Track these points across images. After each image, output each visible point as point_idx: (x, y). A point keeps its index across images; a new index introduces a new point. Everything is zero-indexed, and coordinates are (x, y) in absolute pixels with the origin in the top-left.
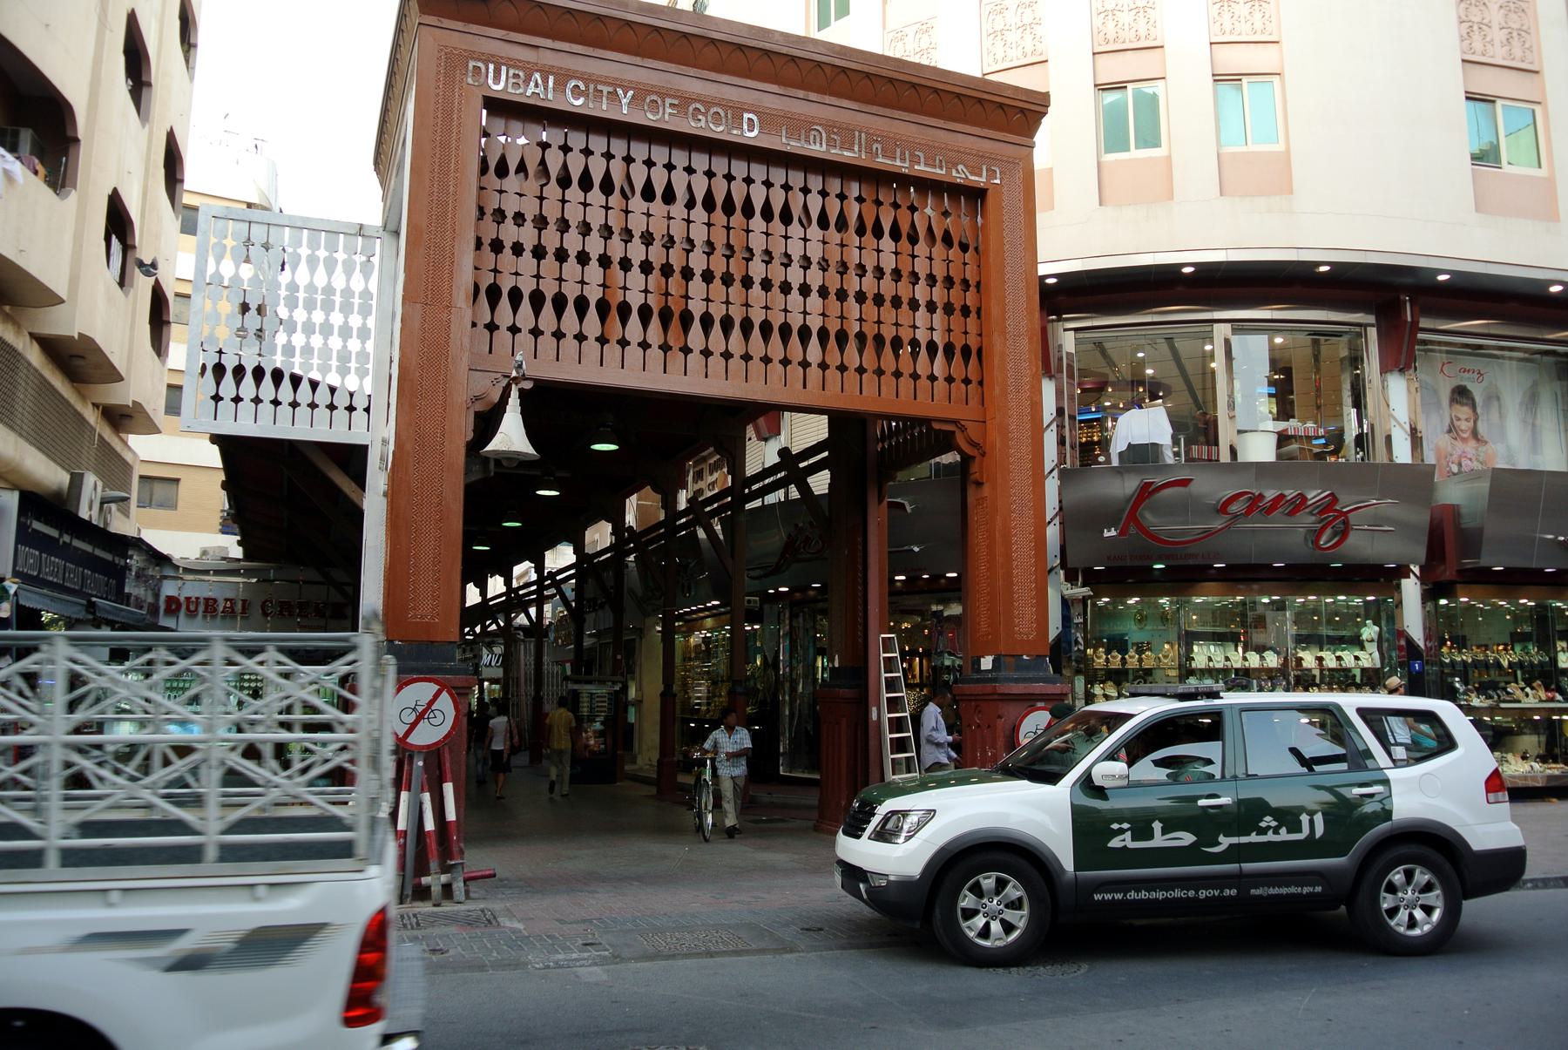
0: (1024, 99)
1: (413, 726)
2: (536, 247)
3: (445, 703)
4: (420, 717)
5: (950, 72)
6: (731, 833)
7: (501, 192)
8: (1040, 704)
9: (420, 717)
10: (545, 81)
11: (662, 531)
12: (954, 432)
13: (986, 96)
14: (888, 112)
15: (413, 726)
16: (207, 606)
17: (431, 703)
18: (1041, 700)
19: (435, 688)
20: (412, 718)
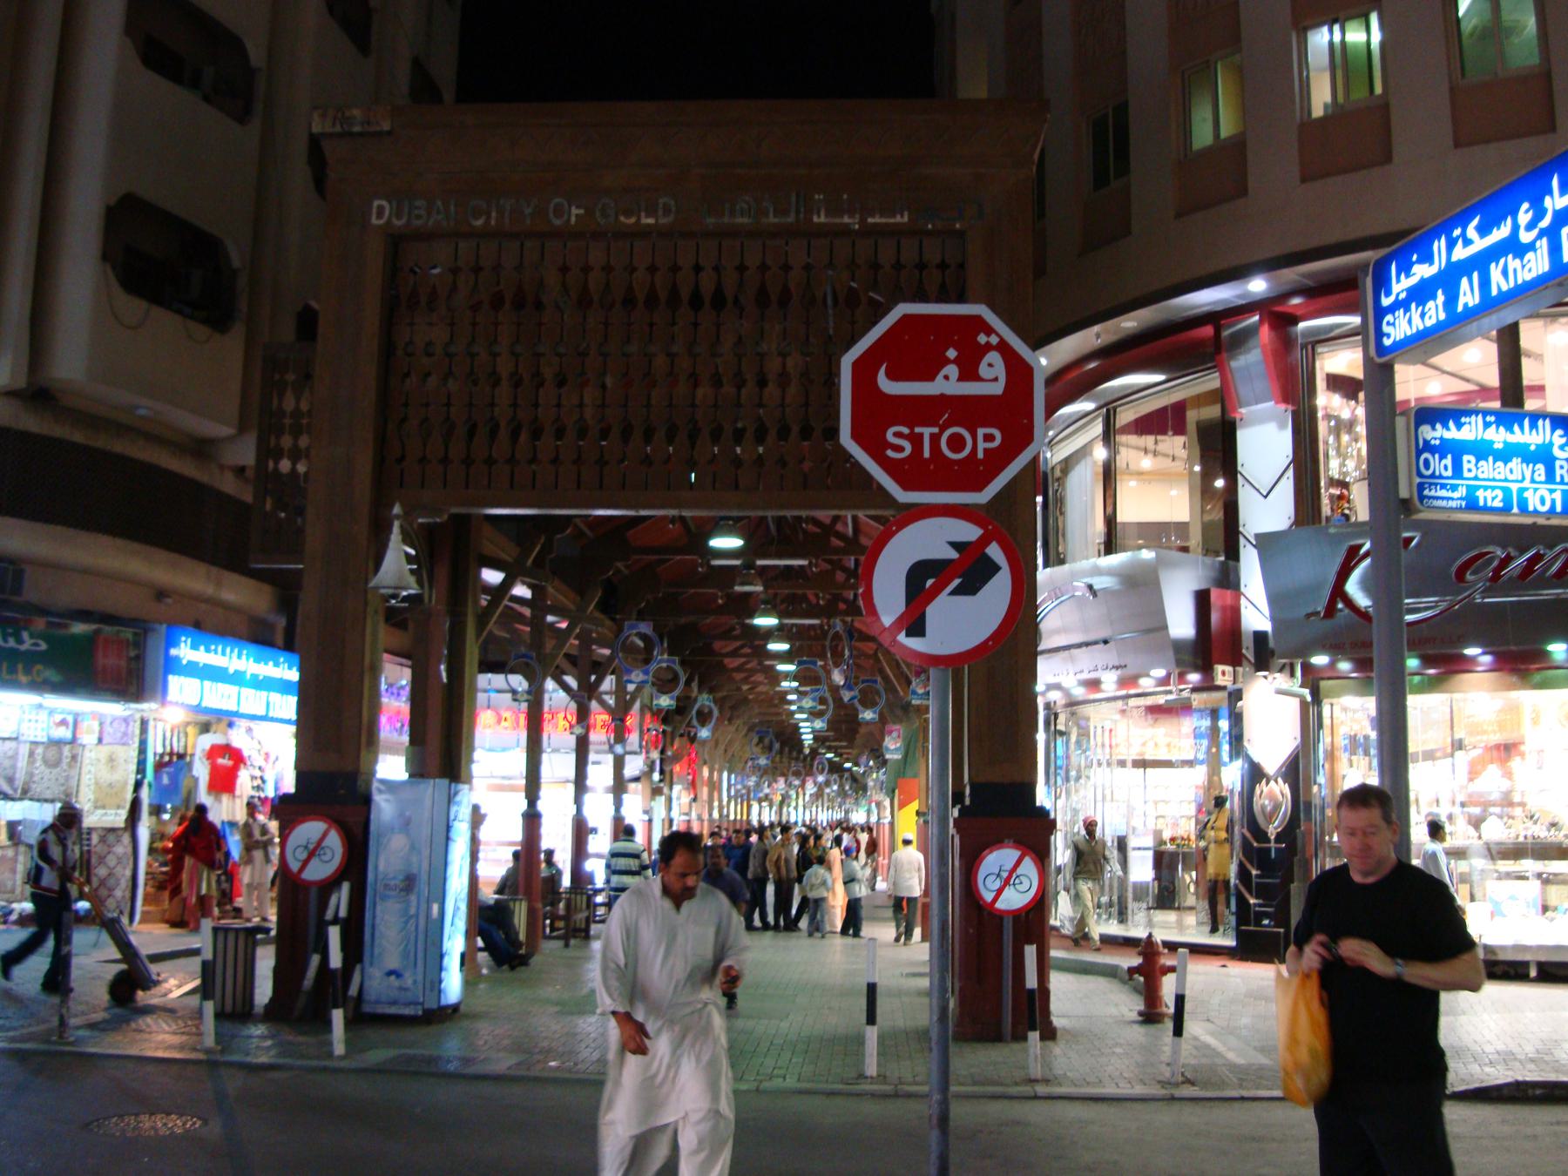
9: (1007, 882)
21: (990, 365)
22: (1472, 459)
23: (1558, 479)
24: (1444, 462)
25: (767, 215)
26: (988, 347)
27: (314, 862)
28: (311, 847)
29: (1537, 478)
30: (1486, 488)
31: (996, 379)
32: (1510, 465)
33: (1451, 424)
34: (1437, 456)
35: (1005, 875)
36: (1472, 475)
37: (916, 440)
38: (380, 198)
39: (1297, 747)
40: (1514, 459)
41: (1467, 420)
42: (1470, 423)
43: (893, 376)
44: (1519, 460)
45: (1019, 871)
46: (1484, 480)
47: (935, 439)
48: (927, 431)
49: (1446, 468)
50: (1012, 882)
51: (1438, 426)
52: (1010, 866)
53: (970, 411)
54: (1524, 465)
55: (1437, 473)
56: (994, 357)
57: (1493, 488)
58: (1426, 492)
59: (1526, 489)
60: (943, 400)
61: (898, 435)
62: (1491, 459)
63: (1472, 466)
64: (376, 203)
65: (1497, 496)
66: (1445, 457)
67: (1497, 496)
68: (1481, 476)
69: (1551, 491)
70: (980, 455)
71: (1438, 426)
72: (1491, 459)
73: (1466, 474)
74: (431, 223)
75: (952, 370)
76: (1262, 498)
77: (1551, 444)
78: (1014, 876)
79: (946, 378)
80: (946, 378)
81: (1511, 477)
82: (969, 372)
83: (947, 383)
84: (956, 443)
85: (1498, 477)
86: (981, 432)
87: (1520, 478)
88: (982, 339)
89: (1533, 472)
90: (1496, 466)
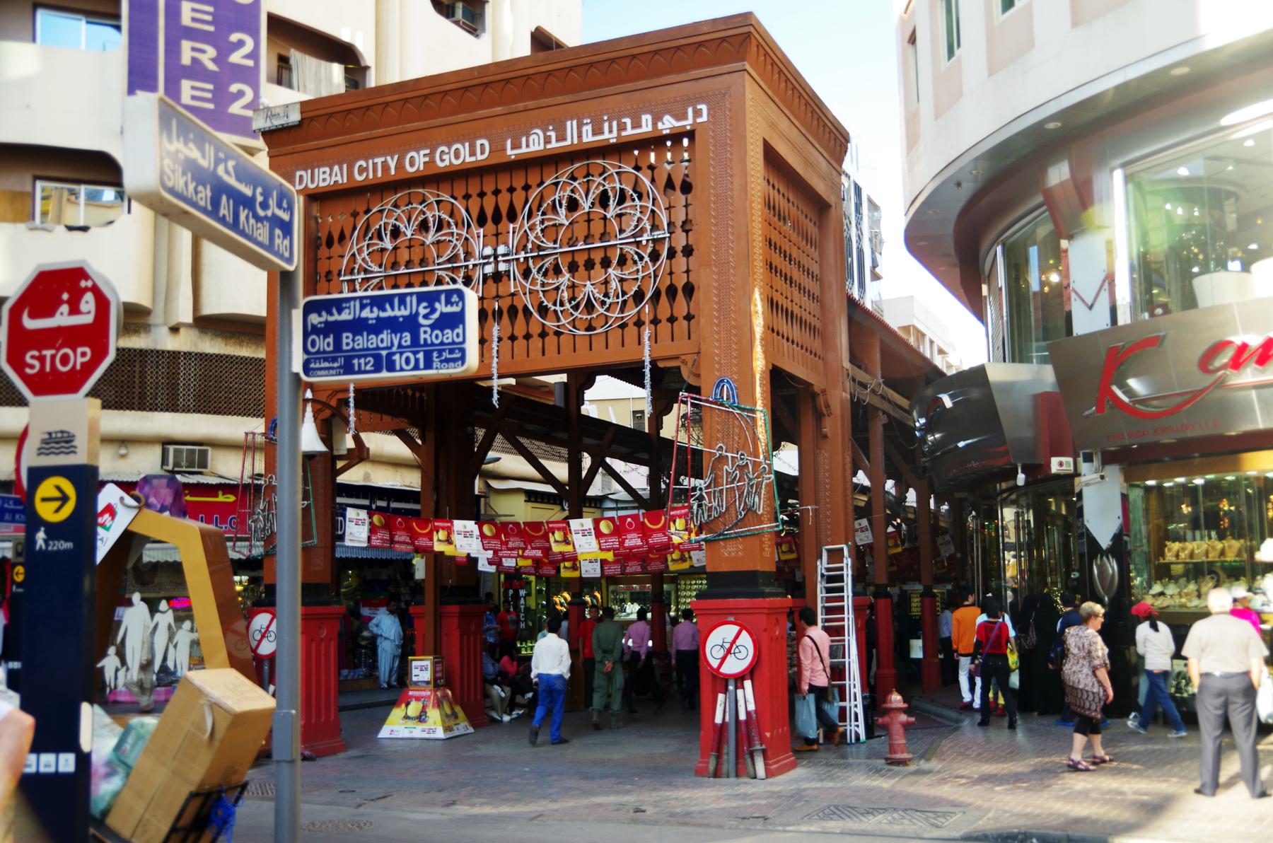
0: (724, 27)
1: (723, 659)
2: (684, 223)
3: (746, 640)
4: (729, 652)
5: (645, 34)
6: (1098, 762)
7: (329, 258)
8: (731, 619)
9: (729, 652)
10: (341, 169)
11: (961, 444)
12: (678, 368)
13: (682, 42)
14: (597, 92)
15: (723, 659)
16: (1242, 528)
17: (734, 642)
18: (731, 614)
19: (737, 628)
20: (721, 653)
21: (87, 302)
22: (350, 335)
23: (422, 342)
24: (327, 340)
25: (625, 129)
26: (86, 289)
27: (265, 641)
28: (263, 631)
29: (404, 343)
30: (359, 357)
31: (89, 312)
32: (381, 336)
33: (334, 311)
34: (322, 337)
35: (727, 646)
36: (349, 347)
37: (42, 359)
38: (300, 170)
39: (1121, 525)
40: (385, 332)
41: (348, 305)
42: (349, 308)
43: (33, 316)
44: (389, 331)
45: (738, 642)
46: (360, 350)
47: (53, 357)
48: (48, 353)
49: (328, 345)
50: (732, 652)
51: (324, 313)
52: (730, 639)
53: (72, 336)
54: (393, 335)
55: (322, 349)
56: (89, 297)
57: (365, 356)
58: (312, 366)
59: (394, 354)
60: (59, 330)
61: (33, 357)
62: (365, 334)
63: (350, 341)
64: (298, 174)
65: (369, 361)
66: (328, 337)
67: (369, 361)
68: (357, 347)
69: (415, 353)
70: (78, 367)
71: (324, 313)
72: (365, 334)
73: (345, 348)
74: (332, 183)
75: (65, 308)
76: (1086, 309)
77: (417, 313)
78: (734, 646)
79: (62, 314)
80: (62, 314)
81: (381, 345)
82: (75, 310)
83: (62, 318)
84: (65, 360)
85: (370, 346)
86: (80, 350)
87: (389, 345)
88: (83, 284)
89: (401, 338)
90: (370, 337)
